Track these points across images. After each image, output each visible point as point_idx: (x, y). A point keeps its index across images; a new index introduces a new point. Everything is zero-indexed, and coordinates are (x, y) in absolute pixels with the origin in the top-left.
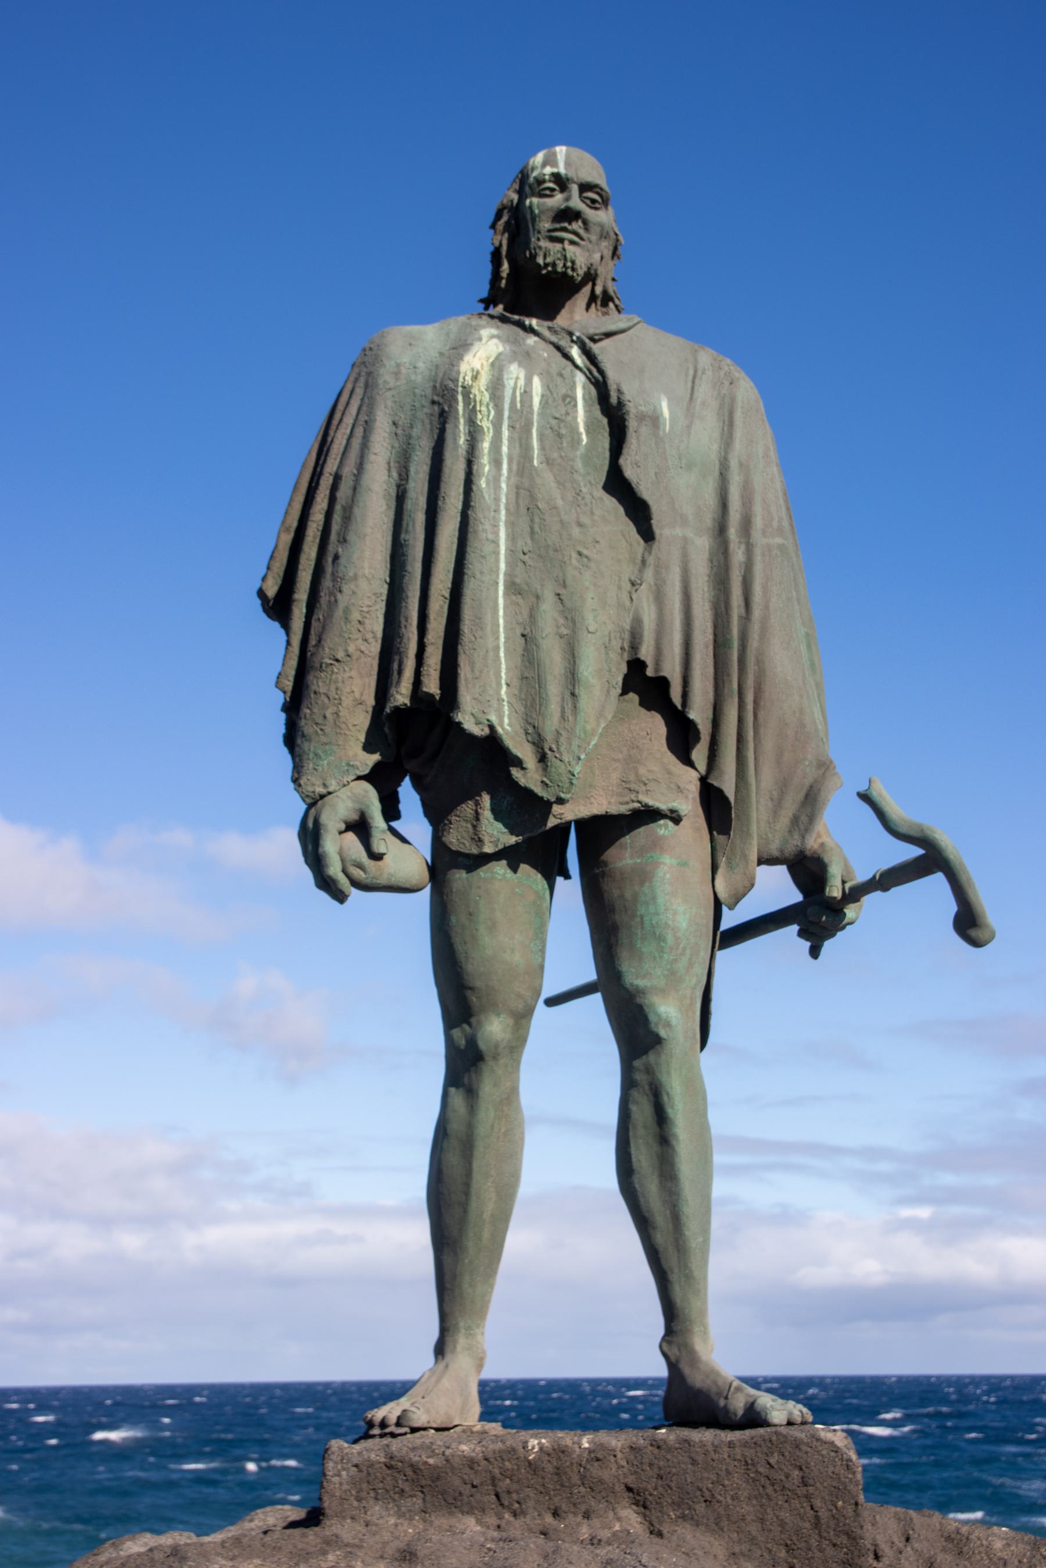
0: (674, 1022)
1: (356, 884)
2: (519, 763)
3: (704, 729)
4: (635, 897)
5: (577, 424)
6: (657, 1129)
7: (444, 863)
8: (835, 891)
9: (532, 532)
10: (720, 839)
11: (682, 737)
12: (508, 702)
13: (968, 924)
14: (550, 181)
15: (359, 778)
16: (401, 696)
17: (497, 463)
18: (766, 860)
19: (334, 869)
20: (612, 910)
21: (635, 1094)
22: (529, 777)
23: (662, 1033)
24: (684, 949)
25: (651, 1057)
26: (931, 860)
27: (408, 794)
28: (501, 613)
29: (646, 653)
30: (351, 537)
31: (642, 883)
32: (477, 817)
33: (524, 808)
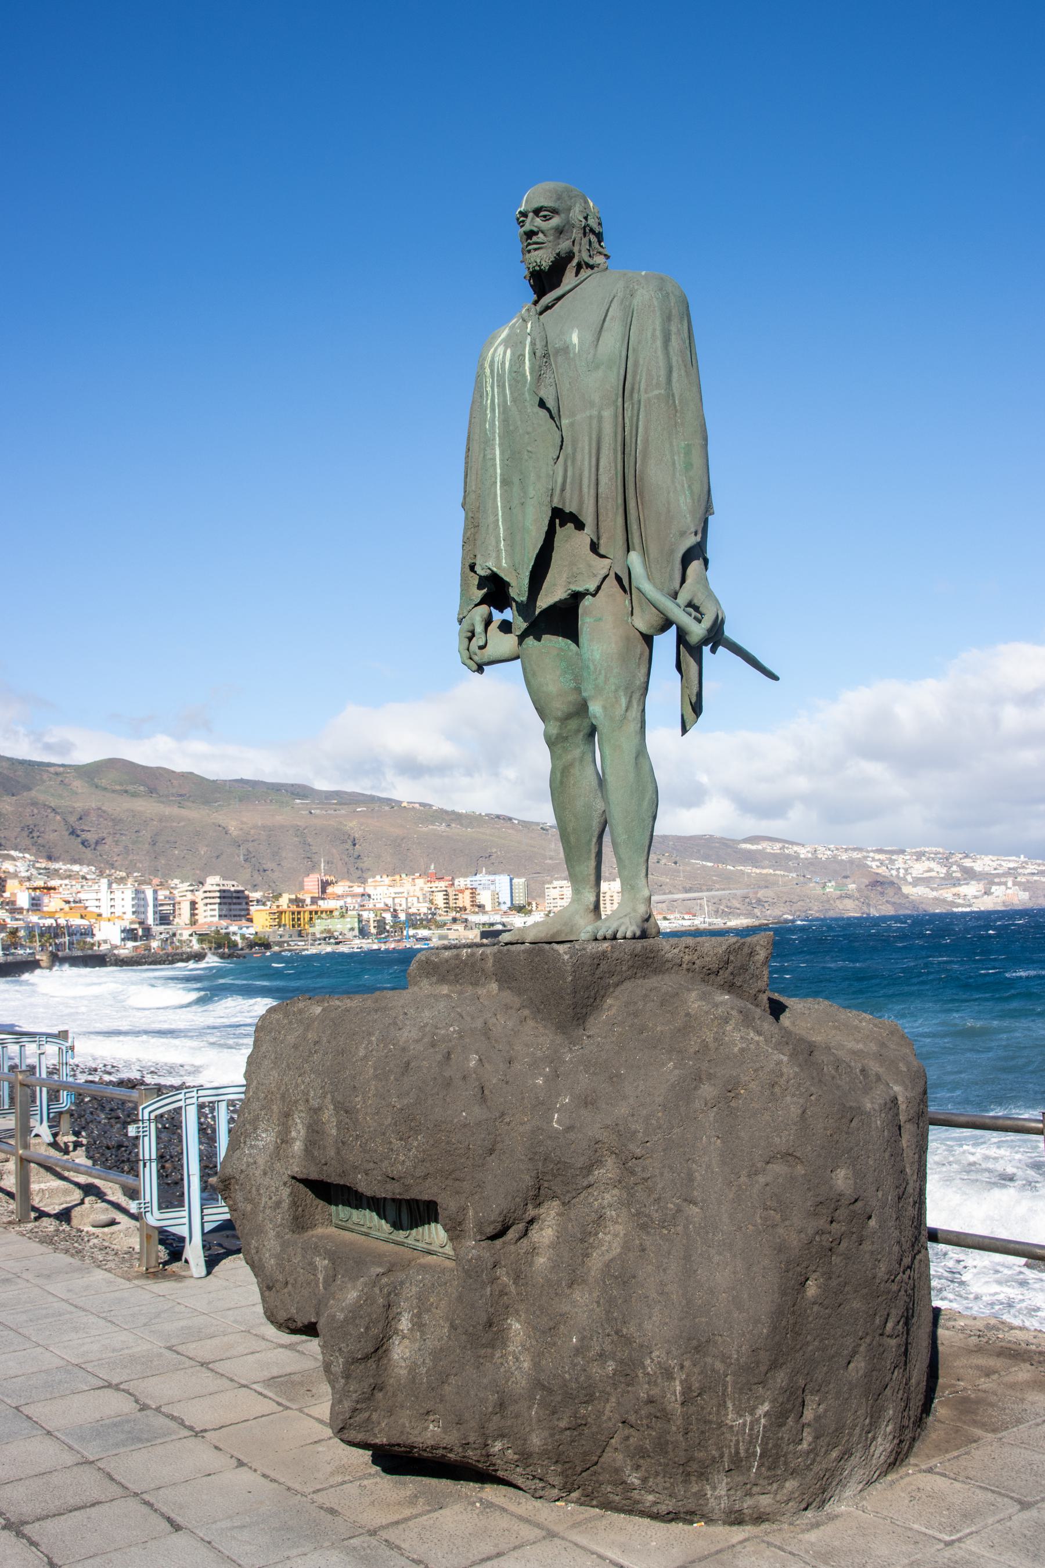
5: (525, 370)
15: (476, 605)
17: (493, 410)
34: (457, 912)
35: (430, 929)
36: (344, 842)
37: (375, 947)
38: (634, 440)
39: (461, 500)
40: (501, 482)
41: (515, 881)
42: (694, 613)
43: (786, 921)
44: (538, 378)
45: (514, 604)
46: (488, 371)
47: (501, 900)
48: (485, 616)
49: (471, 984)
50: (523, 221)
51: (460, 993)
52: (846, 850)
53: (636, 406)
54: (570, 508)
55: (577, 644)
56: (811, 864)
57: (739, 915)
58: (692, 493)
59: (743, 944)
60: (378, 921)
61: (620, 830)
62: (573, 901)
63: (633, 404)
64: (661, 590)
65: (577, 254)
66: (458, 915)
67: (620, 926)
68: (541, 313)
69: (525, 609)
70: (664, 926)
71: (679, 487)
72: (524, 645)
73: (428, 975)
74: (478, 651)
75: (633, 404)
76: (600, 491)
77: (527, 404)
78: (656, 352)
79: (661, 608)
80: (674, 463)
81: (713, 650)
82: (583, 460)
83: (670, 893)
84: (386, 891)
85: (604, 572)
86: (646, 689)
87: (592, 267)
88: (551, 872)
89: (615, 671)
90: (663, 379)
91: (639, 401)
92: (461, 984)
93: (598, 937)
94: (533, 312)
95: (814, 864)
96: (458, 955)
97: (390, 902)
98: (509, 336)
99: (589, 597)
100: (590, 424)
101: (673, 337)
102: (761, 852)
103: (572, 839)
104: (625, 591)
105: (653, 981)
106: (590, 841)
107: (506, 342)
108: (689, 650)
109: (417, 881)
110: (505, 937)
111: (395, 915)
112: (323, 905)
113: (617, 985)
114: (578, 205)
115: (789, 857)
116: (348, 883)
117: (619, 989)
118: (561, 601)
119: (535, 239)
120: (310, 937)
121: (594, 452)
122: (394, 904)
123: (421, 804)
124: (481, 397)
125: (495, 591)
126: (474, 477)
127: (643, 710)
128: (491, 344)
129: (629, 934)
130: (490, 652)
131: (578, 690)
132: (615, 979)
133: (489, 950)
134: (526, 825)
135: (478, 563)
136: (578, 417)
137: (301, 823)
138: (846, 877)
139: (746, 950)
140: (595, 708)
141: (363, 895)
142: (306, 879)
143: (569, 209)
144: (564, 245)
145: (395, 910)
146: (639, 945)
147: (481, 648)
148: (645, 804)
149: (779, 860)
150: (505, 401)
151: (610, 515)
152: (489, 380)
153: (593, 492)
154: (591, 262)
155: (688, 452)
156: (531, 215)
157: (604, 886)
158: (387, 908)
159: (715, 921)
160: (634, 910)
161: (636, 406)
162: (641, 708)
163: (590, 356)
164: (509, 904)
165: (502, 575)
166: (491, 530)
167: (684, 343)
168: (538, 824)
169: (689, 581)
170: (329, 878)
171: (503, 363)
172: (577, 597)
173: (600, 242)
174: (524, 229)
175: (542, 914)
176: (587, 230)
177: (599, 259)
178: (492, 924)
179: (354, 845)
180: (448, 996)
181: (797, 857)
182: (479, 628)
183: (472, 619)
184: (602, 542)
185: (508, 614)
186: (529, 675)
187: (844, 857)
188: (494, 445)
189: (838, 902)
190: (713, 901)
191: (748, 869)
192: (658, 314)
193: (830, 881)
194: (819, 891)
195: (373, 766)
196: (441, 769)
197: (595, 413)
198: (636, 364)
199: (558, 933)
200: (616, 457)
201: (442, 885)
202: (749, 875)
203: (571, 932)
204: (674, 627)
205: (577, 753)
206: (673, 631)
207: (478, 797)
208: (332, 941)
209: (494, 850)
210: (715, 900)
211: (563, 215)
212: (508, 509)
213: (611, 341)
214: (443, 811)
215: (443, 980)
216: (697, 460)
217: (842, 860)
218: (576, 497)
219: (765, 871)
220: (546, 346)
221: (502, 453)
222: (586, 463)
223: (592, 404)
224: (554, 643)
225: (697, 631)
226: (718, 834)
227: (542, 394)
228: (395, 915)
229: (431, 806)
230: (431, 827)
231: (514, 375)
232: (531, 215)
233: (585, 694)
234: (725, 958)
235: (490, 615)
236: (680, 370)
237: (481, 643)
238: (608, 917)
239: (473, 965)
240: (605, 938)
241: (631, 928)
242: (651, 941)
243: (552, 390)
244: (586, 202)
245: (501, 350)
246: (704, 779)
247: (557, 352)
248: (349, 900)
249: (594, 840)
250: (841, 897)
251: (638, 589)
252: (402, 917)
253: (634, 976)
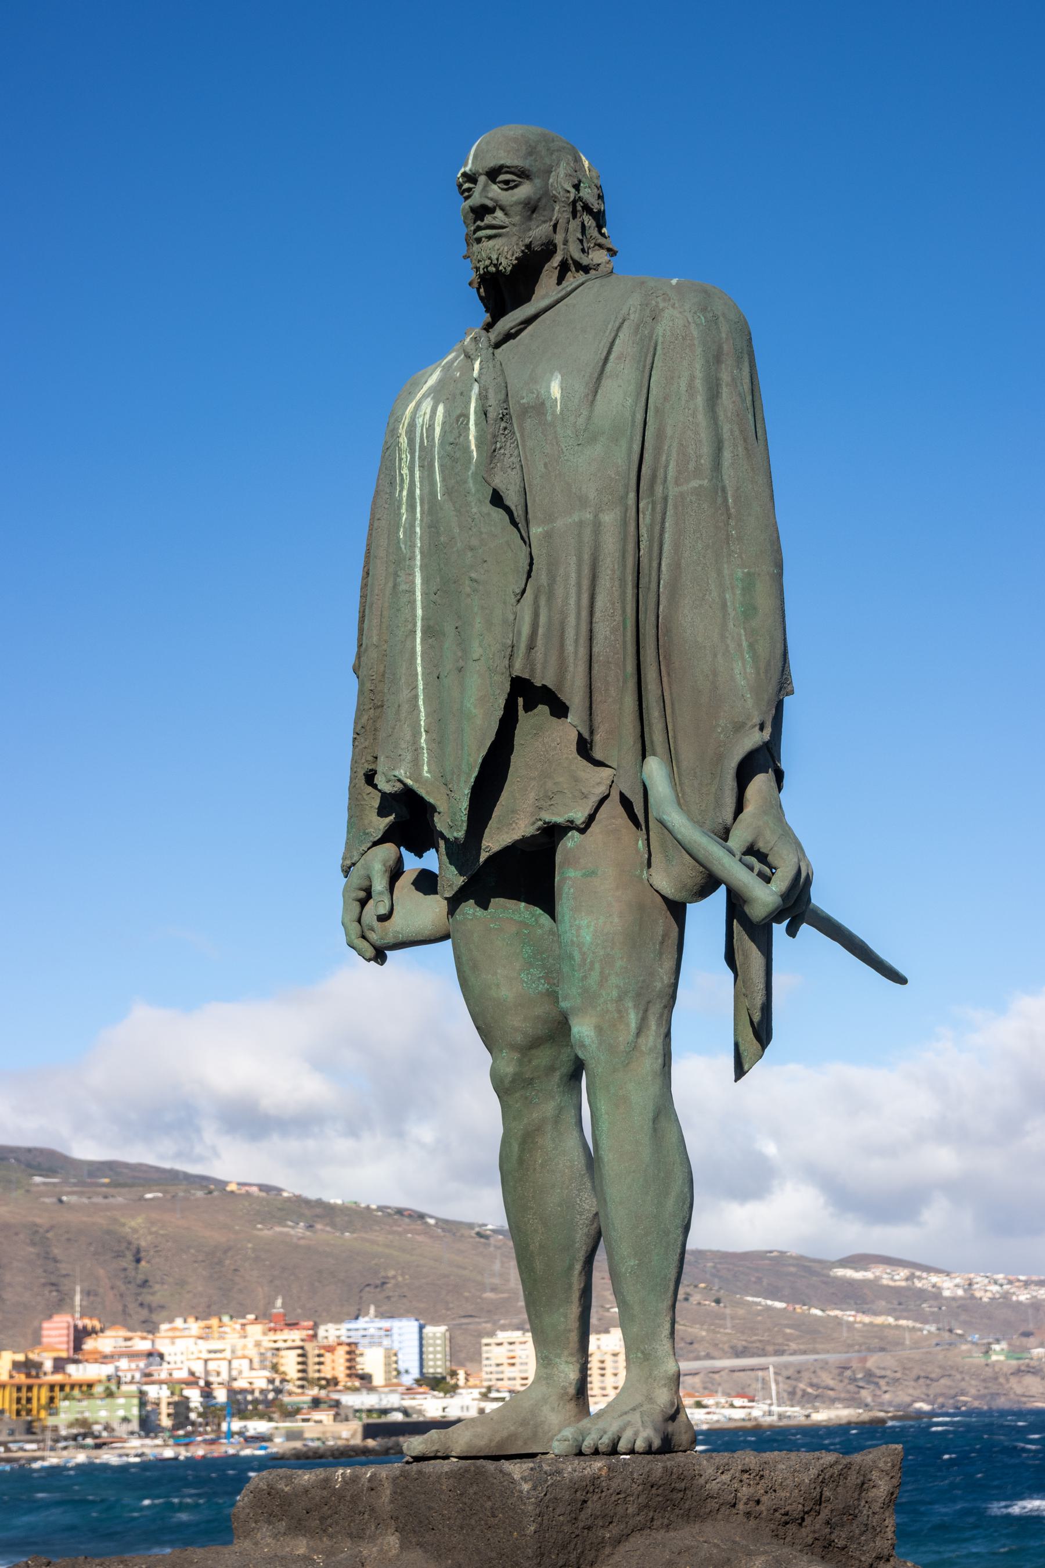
0: (587, 1041)
5: (469, 442)
12: (428, 749)
14: (465, 182)
15: (375, 844)
17: (412, 507)
24: (592, 963)
28: (419, 661)
34: (322, 1387)
35: (271, 1419)
36: (119, 1255)
37: (168, 1453)
38: (655, 564)
39: (352, 659)
40: (424, 632)
41: (429, 1330)
42: (758, 866)
43: (920, 1414)
44: (491, 454)
45: (442, 843)
46: (404, 440)
47: (402, 1366)
48: (391, 863)
49: (350, 1536)
50: (469, 190)
51: (329, 1553)
52: (1027, 1284)
53: (659, 508)
54: (543, 678)
55: (553, 916)
56: (964, 1308)
57: (833, 1401)
58: (755, 657)
59: (848, 1466)
60: (176, 1404)
61: (624, 1249)
62: (538, 1378)
63: (654, 503)
64: (700, 824)
65: (560, 247)
66: (323, 1393)
67: (623, 1429)
68: (497, 345)
69: (461, 853)
70: (698, 1418)
71: (732, 646)
72: (458, 916)
73: (271, 1518)
74: (376, 924)
75: (654, 503)
76: (595, 650)
77: (470, 498)
78: (694, 415)
79: (701, 856)
80: (724, 606)
81: (792, 931)
82: (566, 597)
83: (708, 1357)
84: (193, 1348)
85: (601, 790)
86: (673, 997)
87: (586, 269)
88: (493, 1316)
89: (619, 963)
90: (706, 462)
91: (665, 499)
92: (331, 1537)
93: (584, 1449)
94: (483, 343)
95: (967, 1310)
96: (327, 1480)
97: (199, 1369)
98: (441, 382)
99: (576, 833)
100: (579, 535)
101: (725, 391)
102: (873, 1285)
103: (539, 1265)
104: (637, 824)
105: (684, 1535)
106: (571, 1268)
107: (437, 393)
108: (748, 932)
109: (249, 1328)
110: (414, 1444)
111: (207, 1393)
112: (76, 1372)
113: (618, 1541)
114: (563, 164)
115: (921, 1295)
116: (123, 1333)
117: (623, 1548)
118: (524, 840)
119: (488, 219)
120: (49, 1435)
121: (586, 583)
122: (207, 1373)
123: (262, 1187)
124: (392, 484)
125: (408, 819)
126: (375, 622)
127: (668, 1035)
128: (411, 394)
129: (640, 1445)
130: (401, 924)
131: (552, 996)
132: (615, 1530)
133: (384, 1472)
134: (450, 1227)
135: (380, 769)
136: (559, 523)
137: (42, 1220)
138: (1027, 1334)
139: (853, 1479)
140: (583, 1029)
141: (150, 1354)
142: (46, 1325)
143: (549, 172)
144: (539, 232)
145: (208, 1384)
146: (658, 1465)
147: (383, 918)
148: (670, 1203)
149: (905, 1300)
150: (433, 493)
151: (613, 691)
152: (406, 457)
153: (583, 651)
154: (585, 261)
155: (748, 588)
156: (482, 179)
157: (595, 1341)
158: (192, 1380)
159: (789, 1410)
160: (650, 1399)
161: (659, 508)
162: (663, 1030)
163: (581, 421)
164: (415, 1373)
165: (422, 792)
166: (403, 715)
167: (744, 401)
168: (470, 1226)
169: (749, 809)
170: (88, 1323)
171: (431, 428)
172: (553, 833)
173: (600, 227)
174: (470, 202)
175: (476, 1393)
176: (578, 207)
177: (598, 256)
178: (385, 1412)
179: (138, 1261)
180: (307, 1559)
181: (936, 1294)
182: (379, 885)
183: (368, 867)
184: (597, 738)
185: (431, 861)
186: (466, 968)
187: (1023, 1297)
188: (412, 568)
189: (1013, 1380)
190: (786, 1373)
191: (849, 1316)
192: (699, 350)
193: (998, 1341)
194: (978, 1359)
195: (177, 1115)
196: (301, 1123)
197: (588, 516)
198: (660, 435)
199: (512, 1437)
200: (624, 593)
201: (295, 1336)
202: (850, 1326)
203: (534, 1436)
204: (722, 890)
205: (549, 1108)
206: (720, 896)
207: (365, 1175)
208: (89, 1441)
209: (391, 1273)
210: (790, 1372)
211: (537, 181)
212: (435, 677)
213: (618, 395)
214: (300, 1202)
215: (298, 1528)
216: (764, 602)
217: (1019, 1303)
218: (553, 660)
219: (879, 1320)
220: (506, 400)
221: (426, 581)
222: (572, 601)
223: (583, 502)
224: (512, 913)
225: (764, 897)
226: (794, 1251)
227: (498, 481)
228: (207, 1393)
229: (279, 1190)
230: (278, 1229)
231: (449, 448)
232: (482, 179)
233: (564, 1004)
234: (816, 1494)
235: (400, 861)
236: (735, 446)
237: (383, 910)
238: (601, 1414)
239: (355, 1499)
240: (596, 1452)
241: (642, 1433)
242: (680, 1457)
243: (514, 475)
244: (577, 160)
245: (427, 406)
246: (771, 1149)
247: (525, 411)
248: (123, 1363)
249: (578, 1267)
250: (1018, 1372)
251: (662, 823)
252: (221, 1396)
253: (648, 1525)
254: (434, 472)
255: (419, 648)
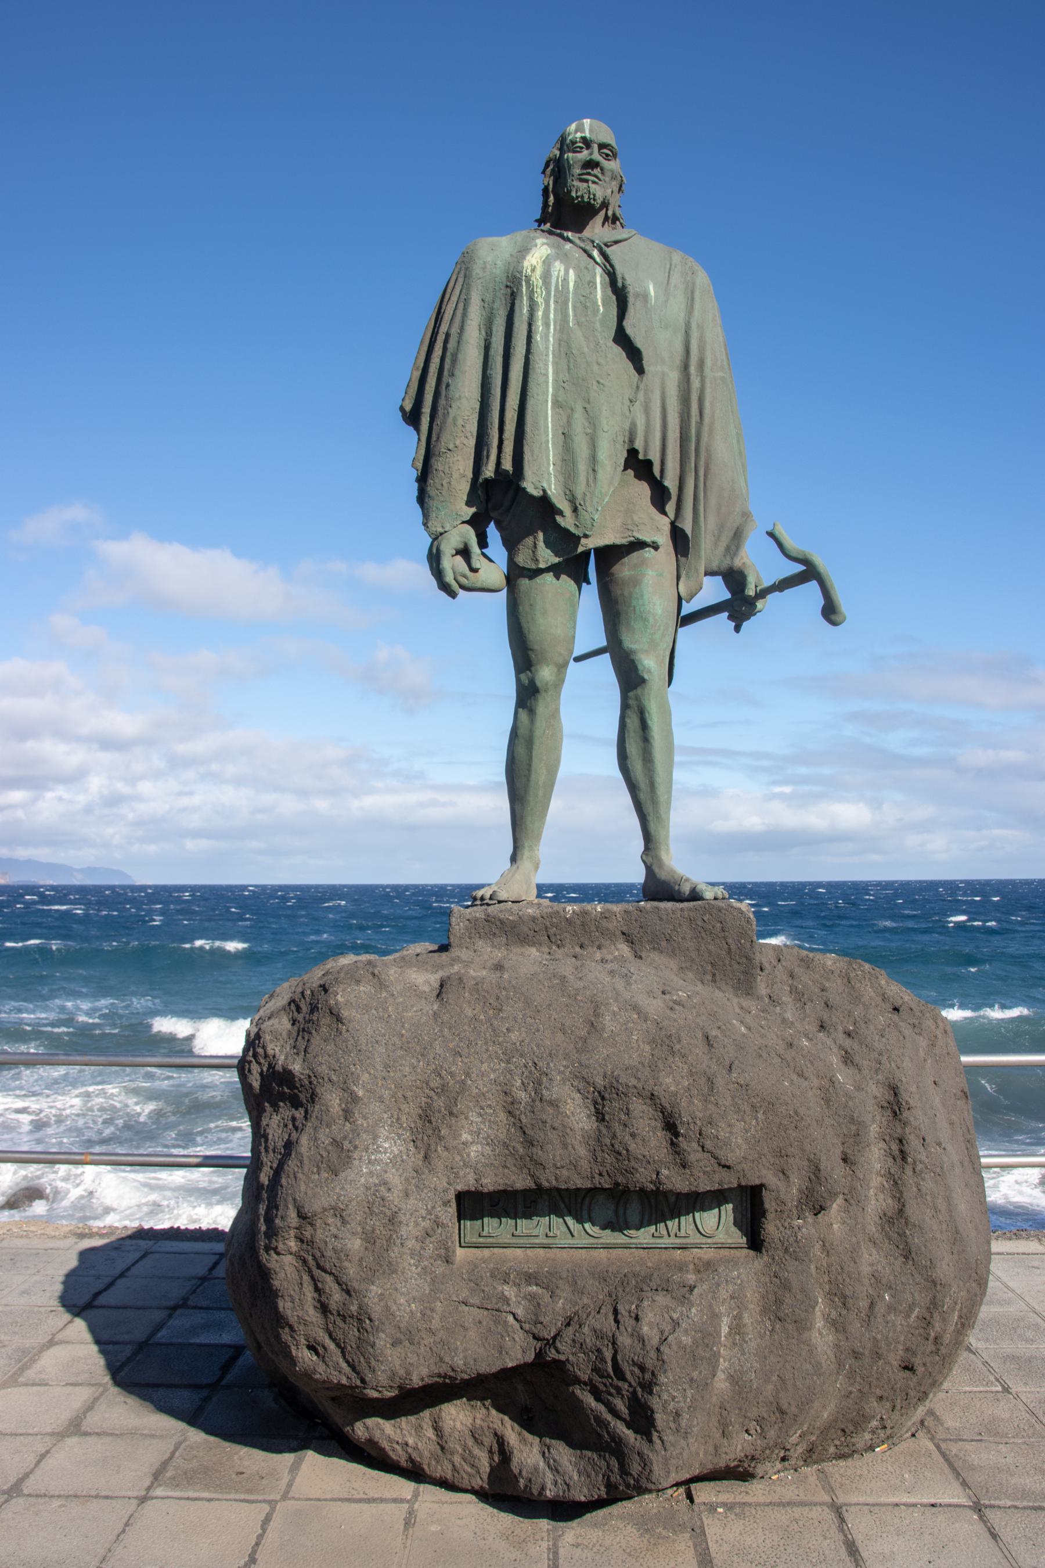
1: (463, 587)
2: (561, 513)
3: (674, 491)
4: (631, 594)
6: (641, 732)
7: (516, 575)
8: (751, 591)
9: (569, 369)
10: (682, 560)
11: (660, 496)
13: (830, 612)
15: (463, 522)
16: (489, 471)
17: (547, 325)
18: (709, 573)
19: (449, 578)
20: (617, 602)
21: (629, 712)
22: (567, 521)
23: (646, 677)
25: (639, 691)
26: (809, 573)
27: (493, 532)
29: (639, 445)
30: (457, 372)
31: (635, 586)
32: (535, 546)
33: (564, 541)
254: (567, 308)
255: (550, 412)
